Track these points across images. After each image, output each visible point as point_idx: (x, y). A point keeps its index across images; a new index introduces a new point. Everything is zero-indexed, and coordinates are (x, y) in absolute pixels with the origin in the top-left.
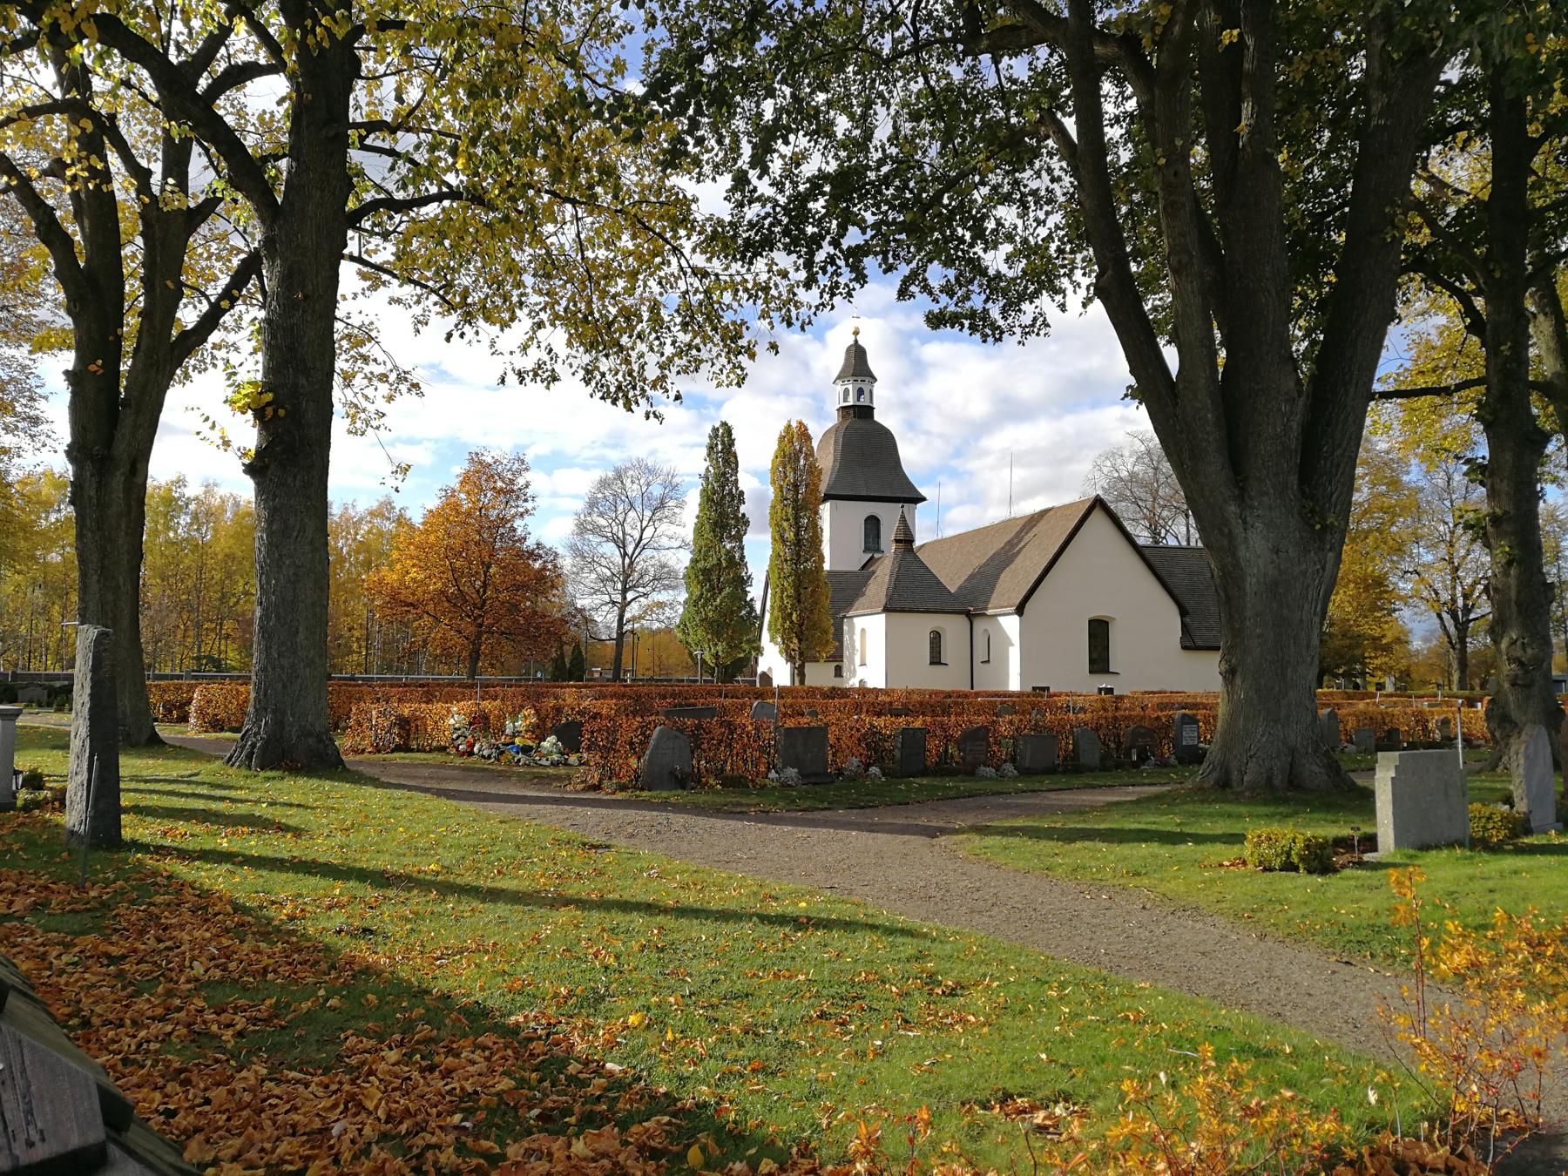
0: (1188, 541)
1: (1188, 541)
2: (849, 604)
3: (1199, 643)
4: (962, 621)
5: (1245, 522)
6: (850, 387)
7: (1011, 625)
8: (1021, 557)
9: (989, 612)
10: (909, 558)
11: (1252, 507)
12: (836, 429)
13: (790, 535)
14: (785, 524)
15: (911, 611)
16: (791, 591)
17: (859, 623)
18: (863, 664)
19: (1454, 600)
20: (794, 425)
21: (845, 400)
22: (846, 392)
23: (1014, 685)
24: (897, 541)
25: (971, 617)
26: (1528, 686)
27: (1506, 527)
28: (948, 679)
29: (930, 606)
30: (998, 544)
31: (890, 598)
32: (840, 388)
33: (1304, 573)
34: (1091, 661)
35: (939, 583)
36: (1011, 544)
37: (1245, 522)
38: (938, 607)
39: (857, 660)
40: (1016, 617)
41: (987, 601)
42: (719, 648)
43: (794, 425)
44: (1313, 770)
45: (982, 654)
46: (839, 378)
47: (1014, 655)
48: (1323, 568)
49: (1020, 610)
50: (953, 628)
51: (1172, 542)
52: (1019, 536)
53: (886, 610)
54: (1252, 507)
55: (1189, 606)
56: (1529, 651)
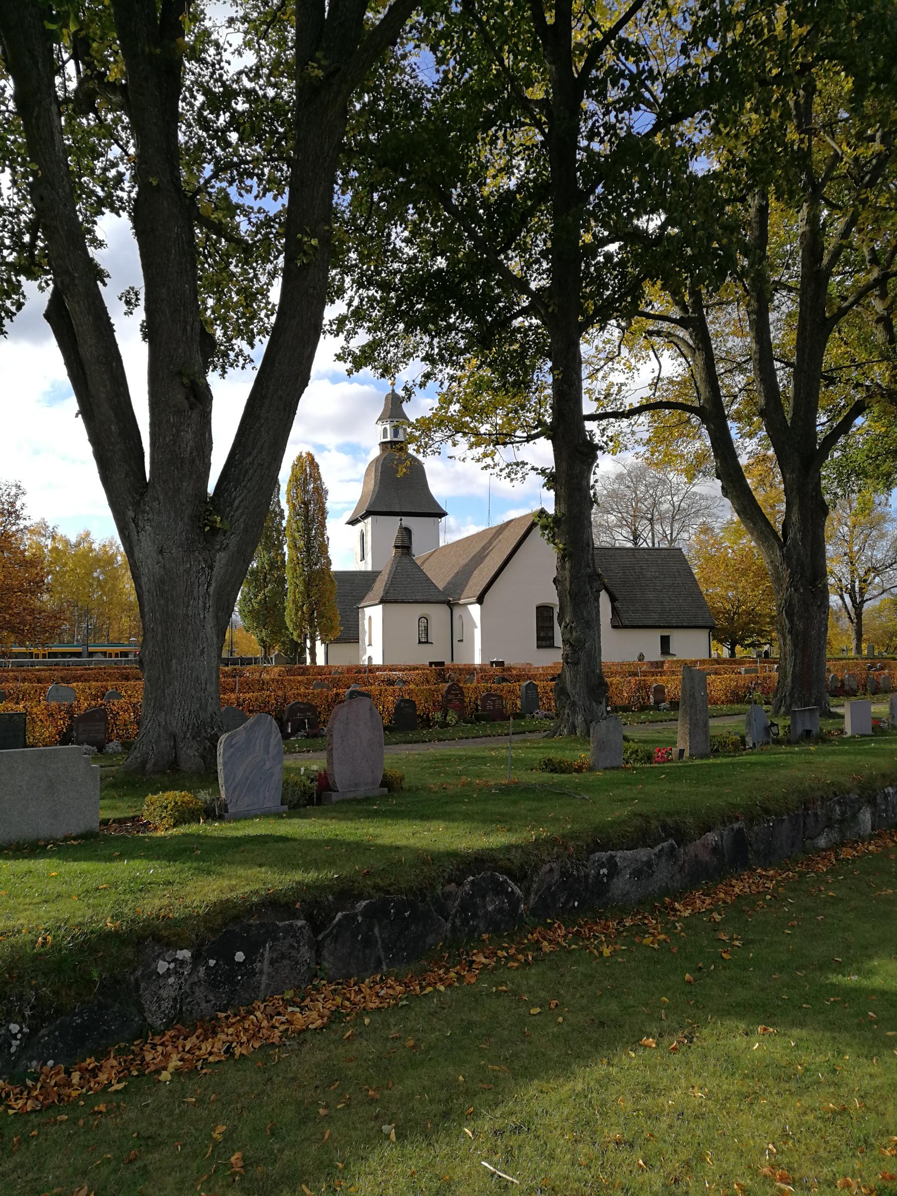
0: (653, 543)
1: (653, 543)
2: (362, 599)
3: (627, 623)
4: (445, 609)
5: (137, 525)
6: (388, 427)
7: (475, 610)
8: (488, 558)
9: (462, 601)
10: (405, 560)
11: (144, 512)
12: (377, 460)
13: (301, 543)
14: (297, 535)
15: (396, 602)
16: (301, 588)
17: (368, 611)
18: (370, 645)
19: (853, 587)
20: (304, 455)
21: (385, 436)
22: (385, 430)
23: (478, 660)
24: (396, 547)
25: (451, 605)
26: (576, 664)
27: (563, 527)
28: (437, 652)
29: (419, 597)
30: (477, 548)
31: (386, 592)
32: (380, 428)
33: (188, 571)
34: (539, 639)
35: (428, 579)
36: (484, 548)
37: (137, 525)
38: (425, 598)
39: (367, 643)
40: (477, 606)
41: (461, 594)
42: (264, 634)
43: (304, 455)
44: (190, 754)
45: (456, 637)
46: (379, 419)
47: (478, 633)
48: (211, 567)
49: (480, 600)
50: (437, 614)
51: (644, 545)
52: (490, 542)
53: (382, 601)
54: (144, 512)
55: (616, 594)
56: (574, 634)
